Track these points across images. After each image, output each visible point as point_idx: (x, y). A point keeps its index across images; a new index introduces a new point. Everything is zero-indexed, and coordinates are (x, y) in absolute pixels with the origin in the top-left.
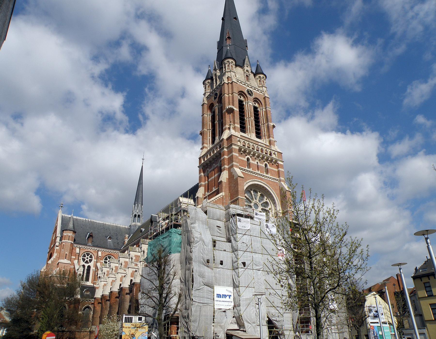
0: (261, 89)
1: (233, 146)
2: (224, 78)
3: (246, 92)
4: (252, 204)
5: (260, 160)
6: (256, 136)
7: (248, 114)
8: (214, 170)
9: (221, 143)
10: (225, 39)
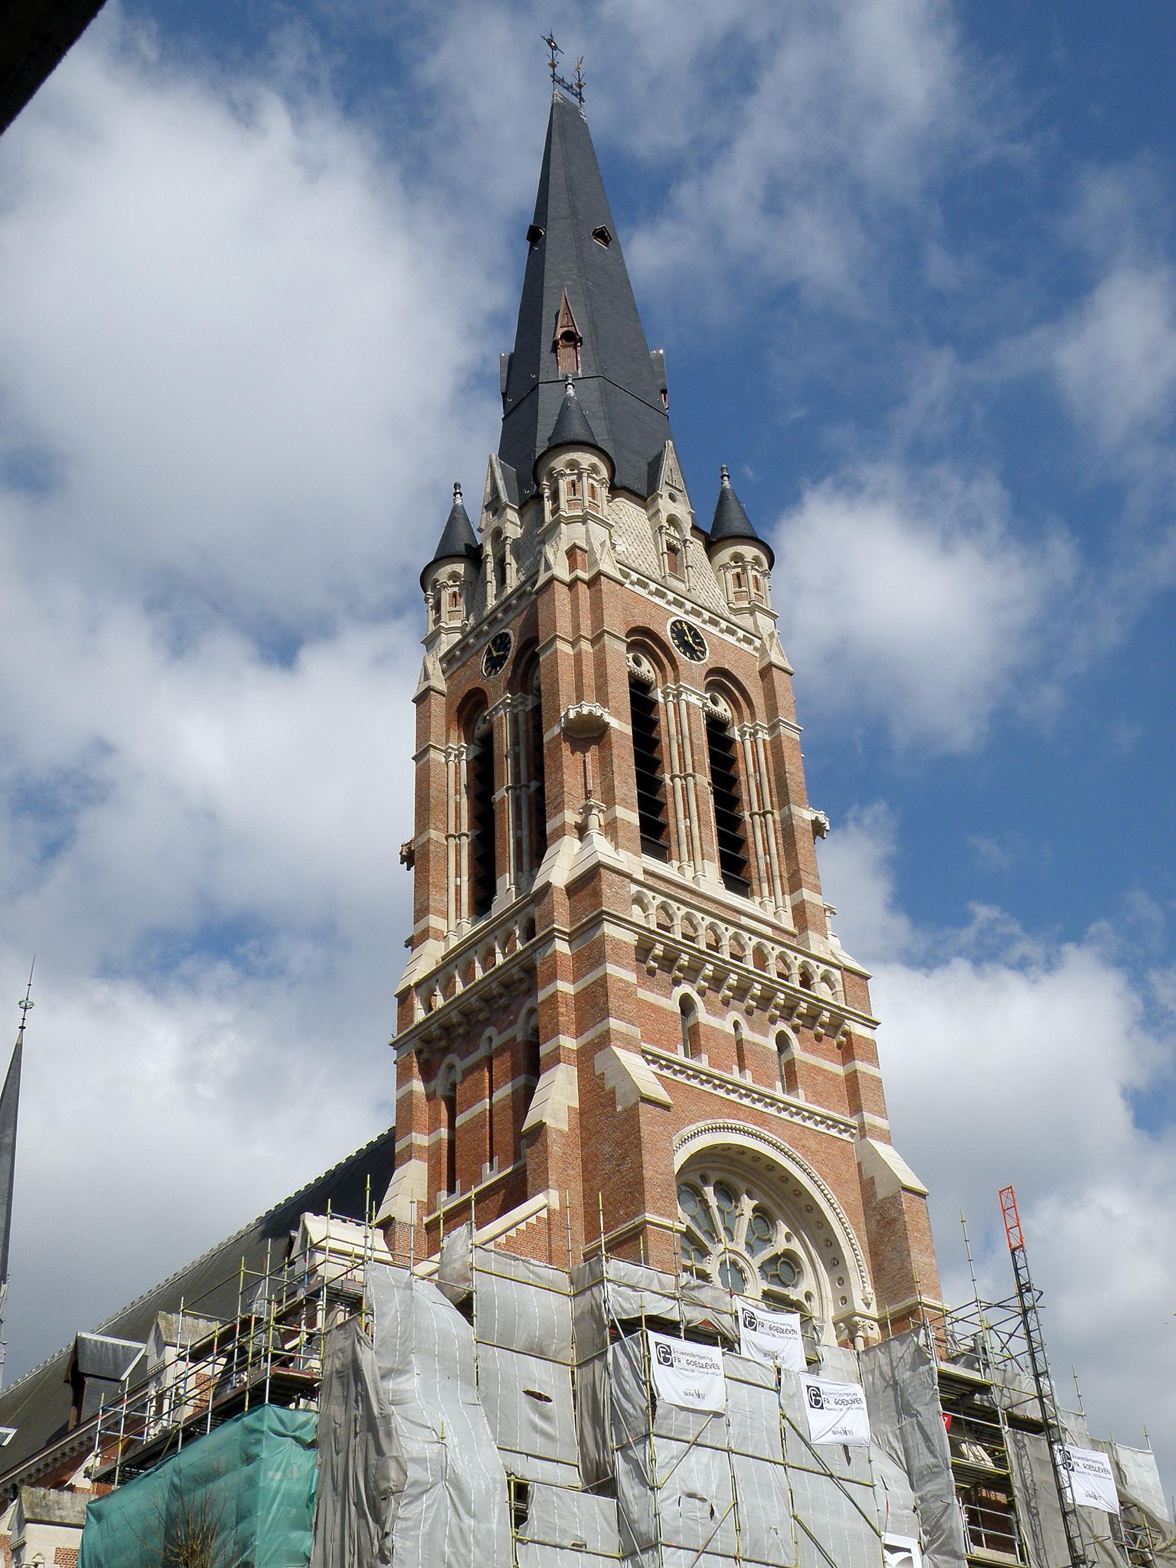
0: (746, 621)
1: (608, 929)
2: (549, 551)
3: (667, 635)
4: (711, 1266)
5: (749, 1012)
6: (724, 876)
7: (682, 755)
8: (489, 1061)
9: (536, 912)
10: (546, 346)
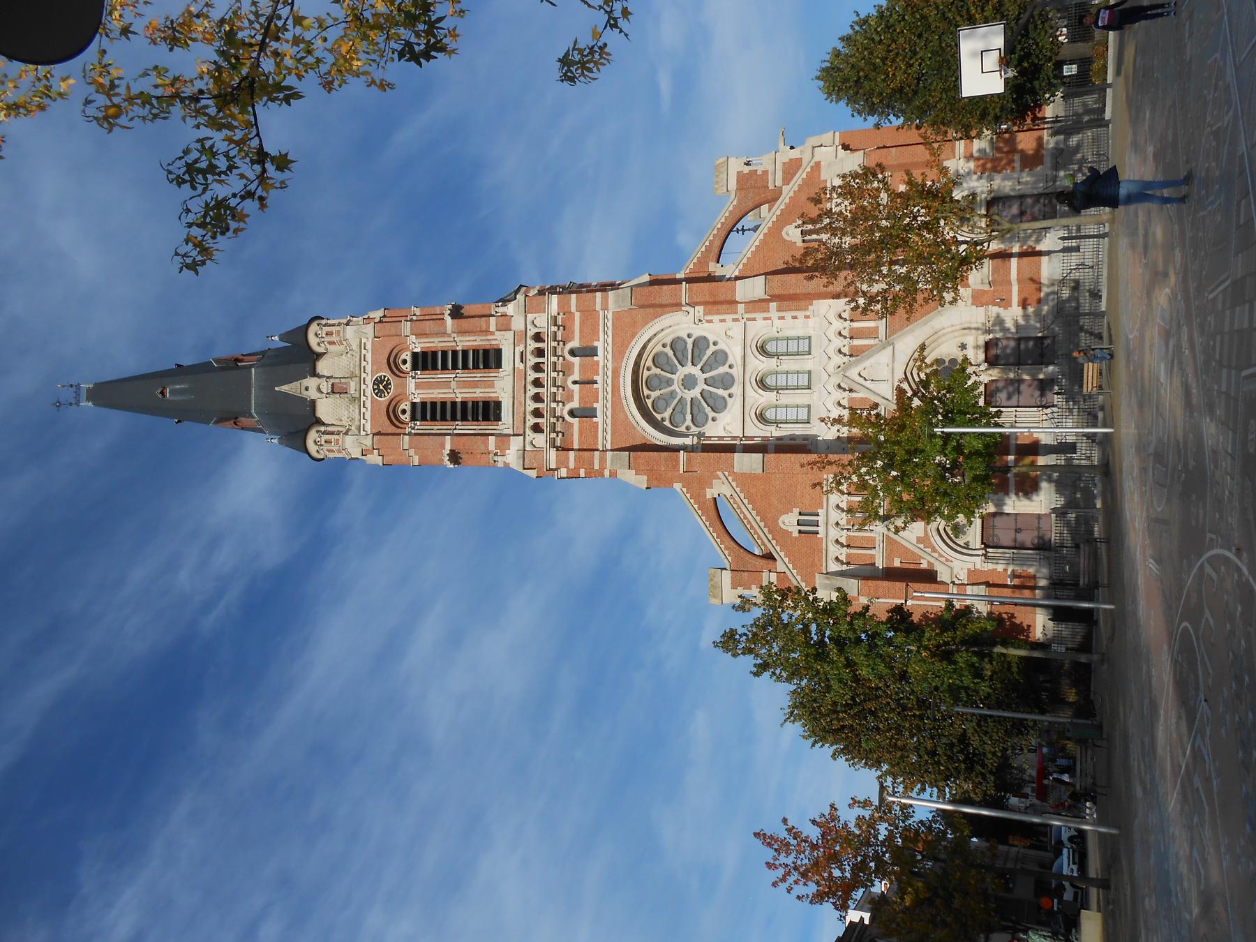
3: (384, 400)
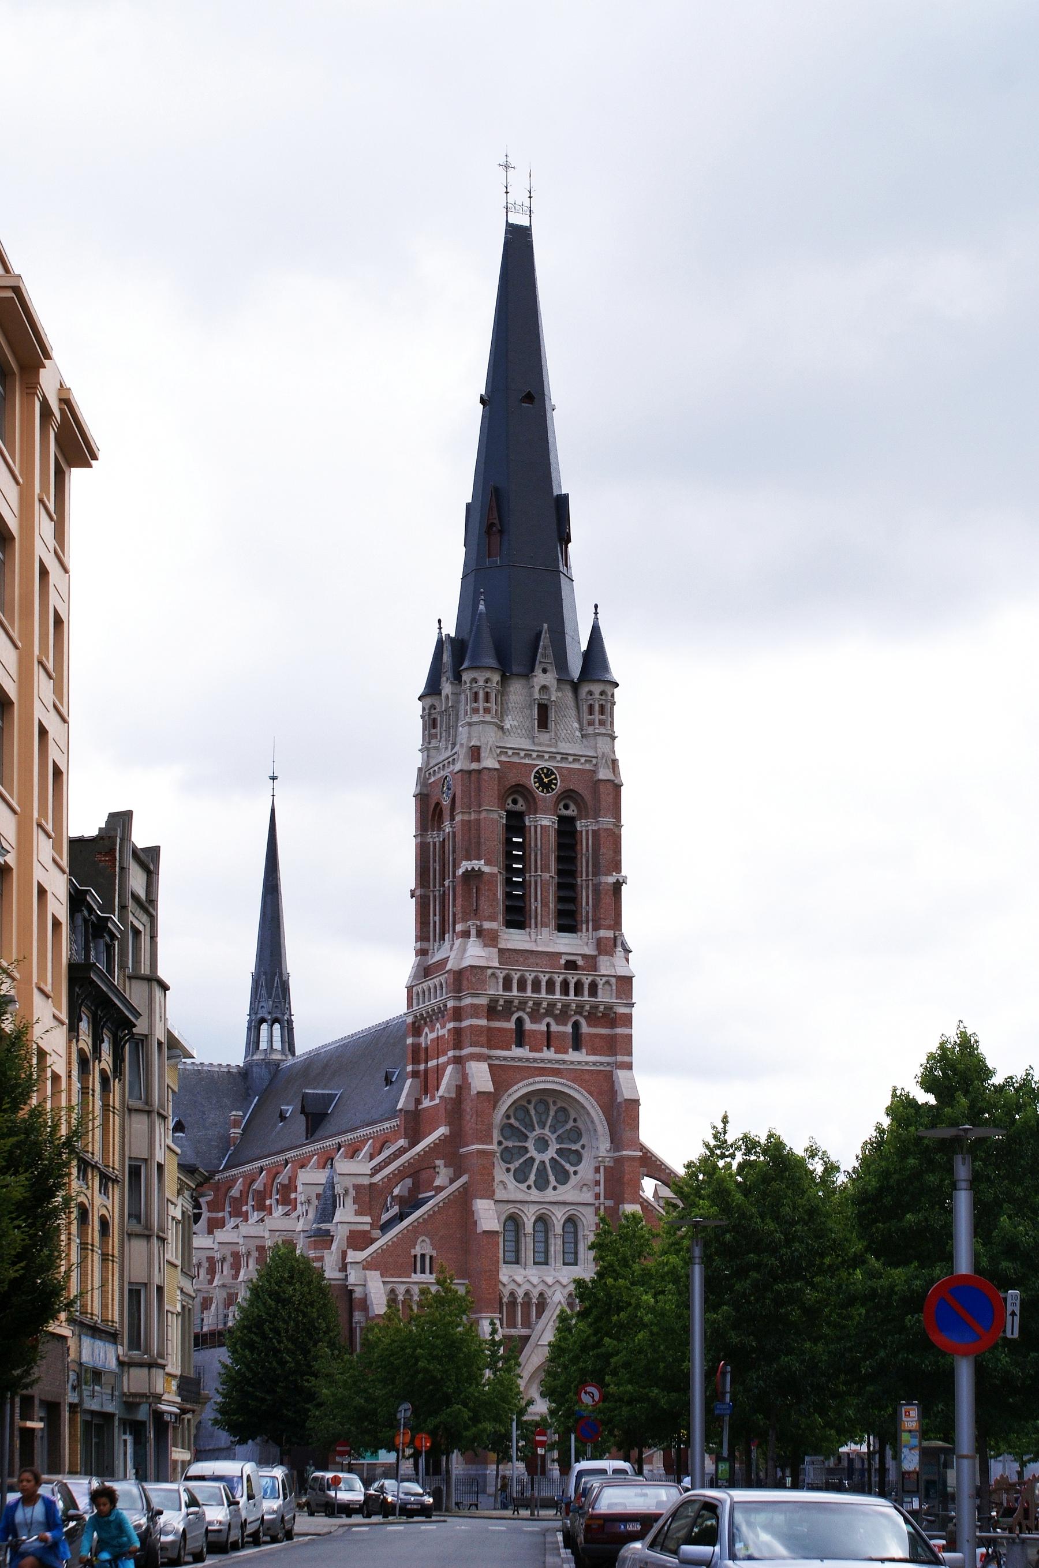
3: (532, 782)
